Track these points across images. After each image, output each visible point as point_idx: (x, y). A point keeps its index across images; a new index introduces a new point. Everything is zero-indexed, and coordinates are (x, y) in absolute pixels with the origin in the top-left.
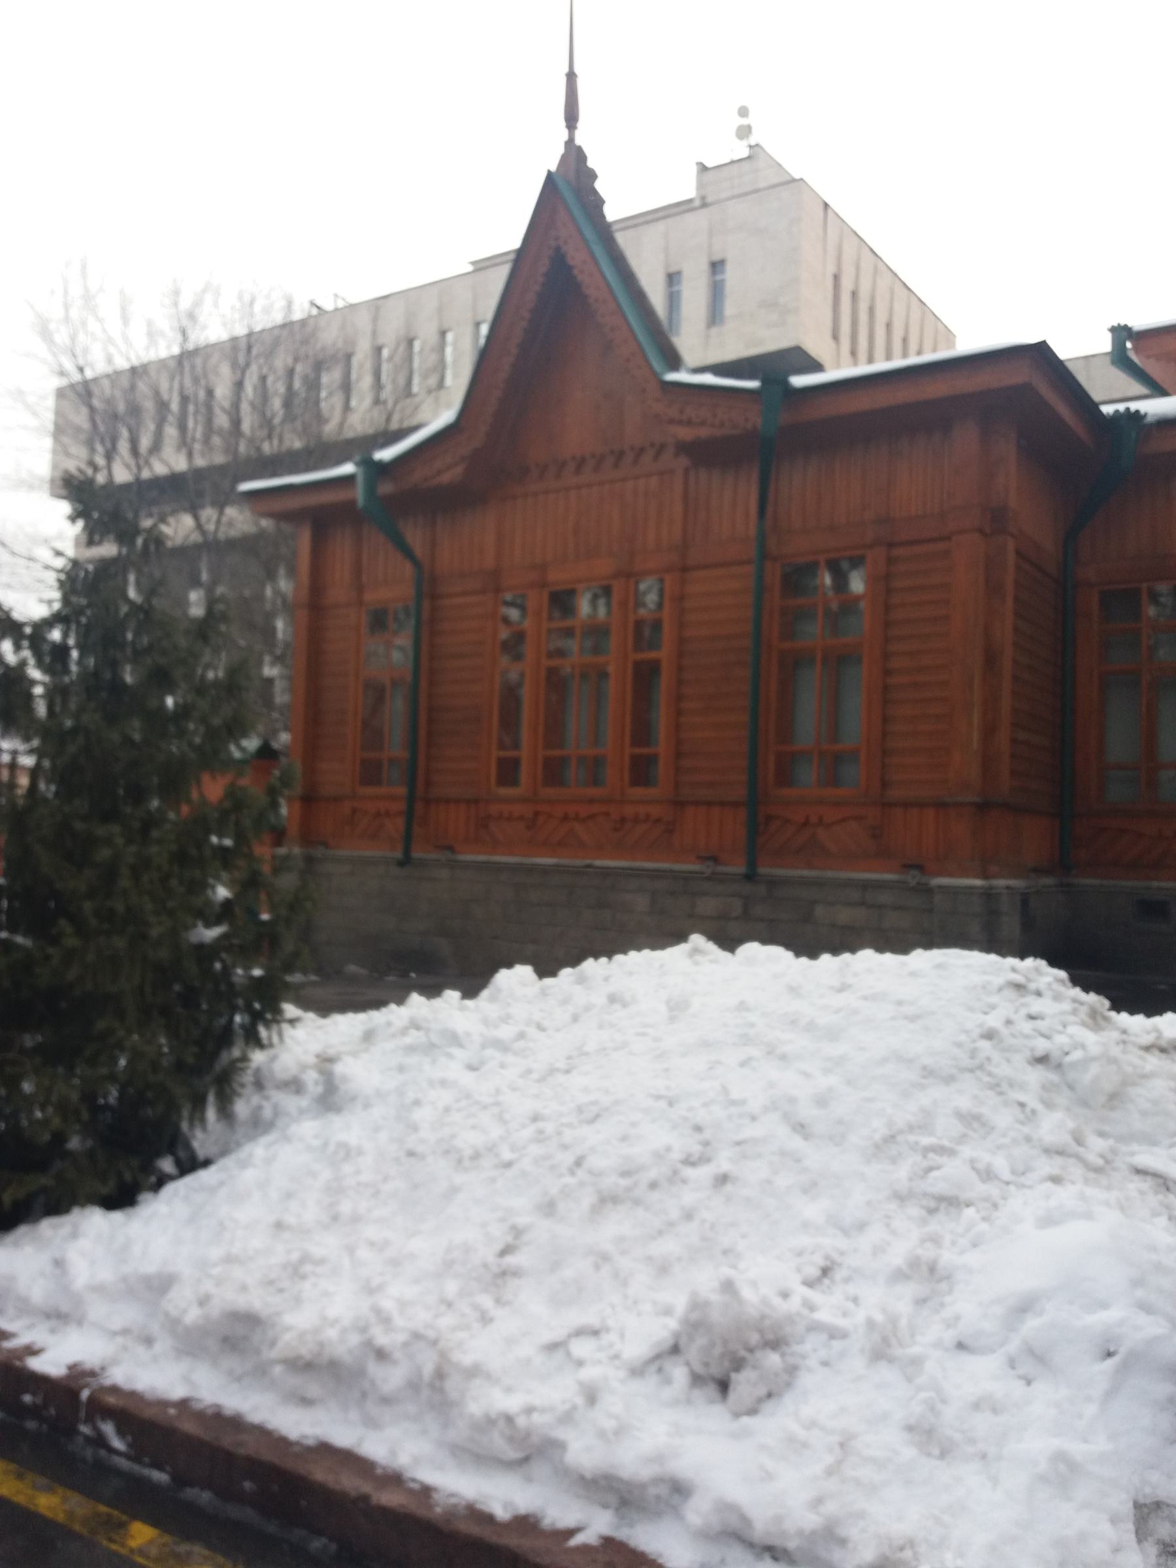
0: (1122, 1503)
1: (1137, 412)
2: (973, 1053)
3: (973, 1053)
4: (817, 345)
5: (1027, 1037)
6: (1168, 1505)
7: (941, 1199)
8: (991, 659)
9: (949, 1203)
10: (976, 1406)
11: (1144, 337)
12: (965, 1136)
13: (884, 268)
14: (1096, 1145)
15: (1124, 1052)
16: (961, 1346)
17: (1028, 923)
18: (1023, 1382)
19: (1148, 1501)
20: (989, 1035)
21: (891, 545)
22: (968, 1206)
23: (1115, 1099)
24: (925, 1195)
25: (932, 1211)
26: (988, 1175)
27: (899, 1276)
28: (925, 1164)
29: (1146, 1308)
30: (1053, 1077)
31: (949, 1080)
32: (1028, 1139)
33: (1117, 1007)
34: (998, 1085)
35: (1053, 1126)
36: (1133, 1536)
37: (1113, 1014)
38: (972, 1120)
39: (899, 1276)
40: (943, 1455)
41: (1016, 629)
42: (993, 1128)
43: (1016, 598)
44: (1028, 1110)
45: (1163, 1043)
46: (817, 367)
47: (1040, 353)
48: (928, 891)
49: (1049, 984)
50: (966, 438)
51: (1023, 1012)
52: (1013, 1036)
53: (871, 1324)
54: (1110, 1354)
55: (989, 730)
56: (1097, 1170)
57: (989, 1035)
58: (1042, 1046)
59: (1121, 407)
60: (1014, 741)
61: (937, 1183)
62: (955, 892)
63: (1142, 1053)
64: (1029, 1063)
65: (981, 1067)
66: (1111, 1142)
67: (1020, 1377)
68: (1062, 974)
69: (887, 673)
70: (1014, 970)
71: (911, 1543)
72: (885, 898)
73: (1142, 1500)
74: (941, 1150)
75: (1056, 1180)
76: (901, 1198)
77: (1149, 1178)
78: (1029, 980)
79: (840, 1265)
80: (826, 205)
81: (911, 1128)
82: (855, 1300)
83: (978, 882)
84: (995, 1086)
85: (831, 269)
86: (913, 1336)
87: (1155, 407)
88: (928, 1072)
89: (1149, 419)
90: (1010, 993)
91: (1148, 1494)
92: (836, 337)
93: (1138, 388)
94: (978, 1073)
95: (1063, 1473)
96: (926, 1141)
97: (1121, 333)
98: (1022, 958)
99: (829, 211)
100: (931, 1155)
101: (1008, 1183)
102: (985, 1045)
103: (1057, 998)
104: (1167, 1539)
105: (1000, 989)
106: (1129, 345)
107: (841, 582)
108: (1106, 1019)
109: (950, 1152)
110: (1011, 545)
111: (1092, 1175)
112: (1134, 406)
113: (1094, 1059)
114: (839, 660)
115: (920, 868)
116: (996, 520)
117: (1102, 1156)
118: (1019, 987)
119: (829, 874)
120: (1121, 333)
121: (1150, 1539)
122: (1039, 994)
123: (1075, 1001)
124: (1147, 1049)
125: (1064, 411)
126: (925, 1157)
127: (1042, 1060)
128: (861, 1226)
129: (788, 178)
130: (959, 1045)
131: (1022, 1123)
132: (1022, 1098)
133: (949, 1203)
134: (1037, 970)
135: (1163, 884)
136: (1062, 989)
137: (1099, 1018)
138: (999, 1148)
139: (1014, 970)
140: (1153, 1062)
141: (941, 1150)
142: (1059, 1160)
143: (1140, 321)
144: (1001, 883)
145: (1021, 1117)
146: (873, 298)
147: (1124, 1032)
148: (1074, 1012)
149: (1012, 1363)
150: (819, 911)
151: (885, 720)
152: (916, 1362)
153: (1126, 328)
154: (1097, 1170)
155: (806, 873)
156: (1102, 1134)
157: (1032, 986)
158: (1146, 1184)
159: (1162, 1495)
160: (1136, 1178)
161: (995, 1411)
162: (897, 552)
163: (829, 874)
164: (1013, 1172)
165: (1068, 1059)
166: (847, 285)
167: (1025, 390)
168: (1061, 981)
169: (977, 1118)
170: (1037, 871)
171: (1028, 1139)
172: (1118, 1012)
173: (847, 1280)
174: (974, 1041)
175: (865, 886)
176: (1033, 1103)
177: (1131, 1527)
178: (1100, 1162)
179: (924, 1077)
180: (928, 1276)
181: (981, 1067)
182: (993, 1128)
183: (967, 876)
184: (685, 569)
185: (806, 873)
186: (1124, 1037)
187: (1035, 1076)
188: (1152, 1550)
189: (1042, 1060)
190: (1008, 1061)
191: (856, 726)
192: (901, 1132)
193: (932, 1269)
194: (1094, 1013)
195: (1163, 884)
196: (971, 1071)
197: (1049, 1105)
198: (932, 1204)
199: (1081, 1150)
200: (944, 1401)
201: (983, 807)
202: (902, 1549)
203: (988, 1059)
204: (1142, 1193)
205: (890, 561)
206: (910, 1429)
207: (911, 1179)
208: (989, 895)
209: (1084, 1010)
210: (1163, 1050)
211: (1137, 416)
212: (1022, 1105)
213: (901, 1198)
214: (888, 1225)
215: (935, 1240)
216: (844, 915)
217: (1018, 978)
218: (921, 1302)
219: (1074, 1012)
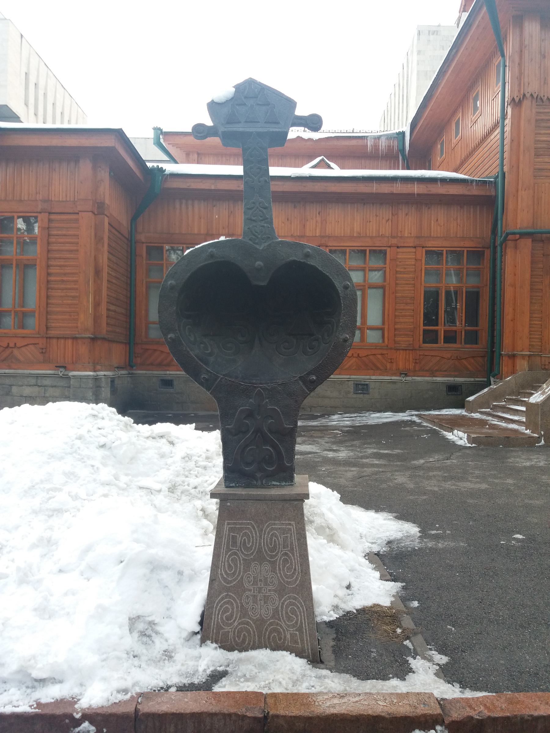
0: (124, 619)
1: (162, 168)
2: (72, 446)
3: (72, 446)
4: (17, 108)
5: (97, 437)
6: (143, 616)
7: (54, 510)
8: (97, 272)
9: (58, 511)
10: (66, 594)
11: (167, 134)
12: (67, 482)
13: (52, 75)
14: (124, 479)
15: (138, 440)
16: (60, 571)
17: (114, 390)
18: (86, 580)
19: (135, 617)
20: (80, 438)
21: (50, 213)
22: (66, 512)
23: (133, 459)
24: (47, 510)
25: (50, 516)
26: (76, 497)
27: (34, 546)
28: (48, 496)
29: (137, 541)
30: (107, 453)
31: (61, 459)
32: (95, 480)
33: (137, 422)
34: (83, 459)
35: (106, 474)
36: (128, 631)
37: (135, 425)
38: (71, 475)
39: (34, 546)
40: (50, 618)
41: (109, 259)
42: (79, 477)
43: (109, 245)
44: (95, 468)
45: (154, 435)
46: (17, 119)
47: (119, 134)
48: (68, 378)
49: (108, 414)
50: (85, 168)
51: (96, 426)
52: (90, 437)
53: (18, 569)
54: (121, 562)
55: (97, 305)
56: (124, 489)
57: (80, 438)
58: (102, 440)
59: (155, 165)
60: (108, 310)
61: (53, 504)
62: (81, 378)
63: (145, 440)
64: (97, 448)
65: (75, 452)
66: (130, 477)
67: (85, 579)
68: (114, 410)
69: (49, 274)
70: (93, 409)
71: (34, 657)
72: (47, 382)
73: (132, 617)
74: (55, 489)
75: (106, 496)
76: (35, 512)
77: (144, 490)
78: (99, 413)
79: (6, 546)
80: (22, 36)
81: (42, 482)
82: (13, 561)
83: (91, 373)
84: (81, 460)
85: (24, 70)
86: (39, 571)
87: (170, 168)
88: (51, 456)
89: (166, 172)
90: (91, 419)
91: (134, 614)
92: (26, 104)
93: (166, 158)
94: (74, 454)
95: (101, 612)
96: (48, 486)
97: (158, 131)
98: (97, 404)
99: (23, 39)
100: (51, 492)
101: (84, 500)
102: (78, 442)
103: (111, 420)
104: (142, 630)
105: (86, 418)
106: (161, 137)
107: (30, 228)
108: (131, 427)
109: (60, 490)
110: (106, 220)
111: (121, 492)
112: (160, 165)
113: (125, 444)
114: (25, 267)
115: (65, 367)
116: (99, 209)
117: (126, 484)
118: (94, 416)
119: (20, 371)
120: (158, 131)
121: (135, 631)
122: (103, 419)
123: (118, 420)
124: (147, 438)
125: (131, 163)
126: (48, 493)
127: (103, 446)
128: (17, 527)
129: (3, 17)
130: (66, 443)
131: (92, 474)
132: (92, 462)
133: (58, 511)
134: (103, 408)
135: (171, 372)
136: (113, 416)
137: (129, 427)
138: (81, 485)
139: (93, 409)
140: (150, 443)
141: (55, 489)
142: (107, 487)
143: (166, 129)
144: (102, 373)
145: (93, 471)
146: (46, 89)
147: (139, 432)
148: (118, 425)
149: (82, 574)
150: (14, 390)
151: (48, 297)
152: (40, 581)
153: (160, 129)
154: (124, 489)
155: (7, 371)
156: (127, 475)
157: (100, 415)
158: (143, 493)
159: (140, 613)
160: (139, 491)
161: (74, 594)
162: (53, 217)
163: (20, 371)
164: (87, 495)
165: (114, 445)
166: (32, 79)
167: (112, 150)
168: (114, 413)
169: (73, 474)
170: (119, 368)
171: (95, 480)
172: (138, 424)
173: (9, 552)
174: (73, 441)
175: (37, 376)
176: (97, 464)
177: (127, 628)
178: (125, 486)
179: (49, 459)
180: (47, 543)
181: (75, 452)
182: (79, 477)
183: (86, 371)
184: (48, 228)
185: (7, 371)
186: (138, 433)
187: (101, 452)
188: (136, 635)
189: (103, 446)
190: (88, 448)
191: (33, 300)
192: (37, 484)
193: (49, 541)
194: (126, 425)
195: (171, 372)
196: (71, 454)
197: (105, 465)
198: (51, 513)
199: (117, 482)
200: (52, 595)
201: (94, 339)
202: (29, 660)
203: (79, 448)
204: (141, 496)
205: (50, 221)
206: (35, 610)
207: (41, 504)
208: (96, 379)
209: (122, 424)
210: (154, 438)
211: (161, 170)
212: (93, 466)
213: (35, 512)
214: (30, 525)
215: (51, 528)
216: (27, 391)
217: (95, 413)
218: (43, 556)
219: (118, 425)
